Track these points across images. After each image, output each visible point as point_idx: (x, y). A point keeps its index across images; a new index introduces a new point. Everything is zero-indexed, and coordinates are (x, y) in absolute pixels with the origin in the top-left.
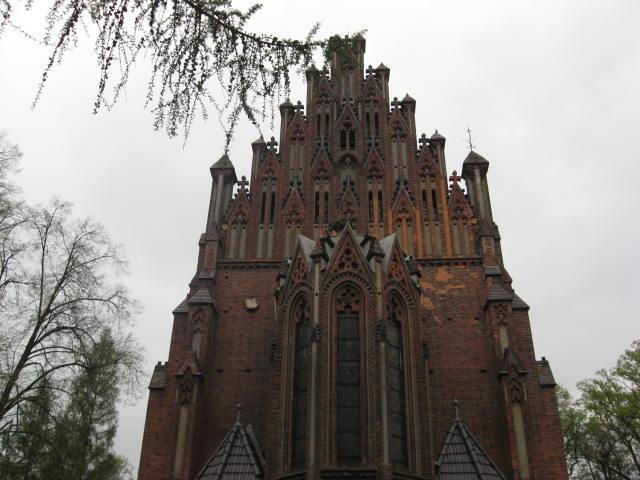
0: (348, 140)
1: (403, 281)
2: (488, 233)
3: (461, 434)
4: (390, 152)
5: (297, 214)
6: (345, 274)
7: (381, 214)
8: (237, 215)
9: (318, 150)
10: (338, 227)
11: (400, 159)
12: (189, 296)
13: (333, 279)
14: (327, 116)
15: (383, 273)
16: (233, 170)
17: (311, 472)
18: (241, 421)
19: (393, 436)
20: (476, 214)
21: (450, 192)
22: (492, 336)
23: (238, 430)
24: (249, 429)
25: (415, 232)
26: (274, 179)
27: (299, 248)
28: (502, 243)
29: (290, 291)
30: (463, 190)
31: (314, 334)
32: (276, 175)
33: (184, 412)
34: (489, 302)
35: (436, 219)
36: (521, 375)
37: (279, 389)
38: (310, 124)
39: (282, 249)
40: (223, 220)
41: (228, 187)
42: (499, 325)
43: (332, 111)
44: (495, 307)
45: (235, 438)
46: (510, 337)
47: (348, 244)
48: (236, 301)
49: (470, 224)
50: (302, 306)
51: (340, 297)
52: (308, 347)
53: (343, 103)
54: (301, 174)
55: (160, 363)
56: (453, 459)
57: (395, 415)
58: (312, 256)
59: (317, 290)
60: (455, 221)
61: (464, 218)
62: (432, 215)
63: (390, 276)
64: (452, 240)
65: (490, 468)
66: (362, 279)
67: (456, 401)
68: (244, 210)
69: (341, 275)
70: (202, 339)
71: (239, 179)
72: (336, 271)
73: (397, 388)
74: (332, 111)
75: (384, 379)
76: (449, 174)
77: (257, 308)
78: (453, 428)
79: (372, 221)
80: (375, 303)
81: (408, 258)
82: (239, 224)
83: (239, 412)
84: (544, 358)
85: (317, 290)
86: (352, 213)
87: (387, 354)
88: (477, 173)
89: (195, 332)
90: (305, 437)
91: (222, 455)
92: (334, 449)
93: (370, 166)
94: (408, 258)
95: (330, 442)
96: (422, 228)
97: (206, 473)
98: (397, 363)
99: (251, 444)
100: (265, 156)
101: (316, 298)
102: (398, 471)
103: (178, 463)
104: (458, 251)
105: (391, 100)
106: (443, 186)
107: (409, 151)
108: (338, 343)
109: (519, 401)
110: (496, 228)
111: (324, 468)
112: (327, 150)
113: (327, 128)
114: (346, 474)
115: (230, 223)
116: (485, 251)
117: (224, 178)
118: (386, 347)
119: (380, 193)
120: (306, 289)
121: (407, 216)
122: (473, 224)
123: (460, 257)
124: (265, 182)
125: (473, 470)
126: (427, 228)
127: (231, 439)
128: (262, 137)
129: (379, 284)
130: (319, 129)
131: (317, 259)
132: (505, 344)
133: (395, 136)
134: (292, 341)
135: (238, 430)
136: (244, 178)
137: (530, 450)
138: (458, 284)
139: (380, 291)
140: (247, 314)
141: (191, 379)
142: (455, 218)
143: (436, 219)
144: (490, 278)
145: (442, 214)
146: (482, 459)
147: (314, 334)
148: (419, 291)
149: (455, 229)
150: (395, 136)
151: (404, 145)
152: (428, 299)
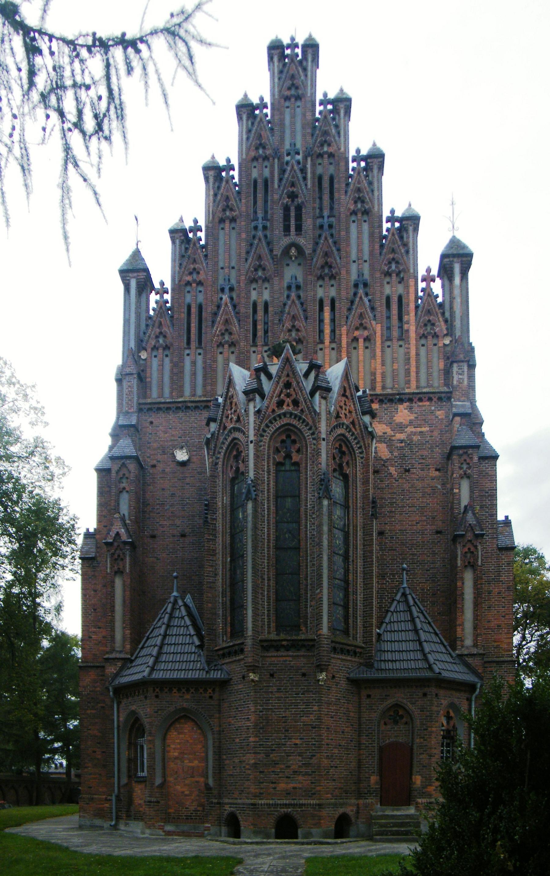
0: (293, 222)
1: (353, 423)
2: (462, 356)
3: (407, 601)
4: (348, 239)
5: (230, 334)
6: (285, 414)
7: (333, 331)
8: (157, 337)
9: (254, 237)
10: (276, 351)
11: (360, 250)
12: (111, 448)
13: (271, 422)
14: (266, 182)
15: (328, 413)
16: (147, 270)
17: (249, 642)
18: (178, 591)
19: (334, 604)
20: (450, 332)
21: (421, 298)
22: (452, 489)
23: (175, 602)
24: (188, 599)
25: (374, 356)
26: (200, 283)
27: (230, 383)
28: (478, 371)
29: (221, 439)
30: (437, 296)
31: (249, 492)
32: (202, 277)
33: (118, 582)
34: (453, 448)
35: (400, 339)
36: (477, 536)
37: (215, 555)
38: (243, 196)
39: (214, 384)
40: (141, 345)
41: (144, 296)
42: (462, 478)
43: (272, 173)
44: (460, 456)
45: (173, 609)
46: (472, 491)
47: (288, 375)
48: (164, 453)
49: (441, 345)
50: (237, 457)
51: (278, 445)
52: (243, 506)
53: (288, 158)
54: (233, 273)
55: (88, 530)
56: (396, 627)
57: (337, 582)
58: (246, 393)
59: (252, 437)
60: (423, 341)
61: (436, 336)
62: (395, 333)
63: (338, 416)
64: (418, 367)
65: (433, 635)
66: (304, 421)
67: (405, 566)
68: (165, 329)
69: (279, 416)
70: (130, 500)
71: (157, 286)
72: (273, 411)
73: (341, 552)
74: (272, 173)
75: (325, 543)
76: (421, 272)
77: (189, 460)
78: (399, 595)
79: (322, 342)
80: (318, 453)
81: (360, 393)
82: (161, 351)
83: (175, 581)
84: (507, 517)
85: (252, 437)
86: (298, 330)
87: (330, 514)
88: (457, 268)
89: (121, 492)
90: (243, 607)
91: (160, 627)
92: (273, 618)
93: (321, 262)
94: (360, 393)
95: (268, 611)
96: (383, 351)
97: (146, 645)
98: (342, 523)
99: (190, 614)
100: (187, 249)
101: (251, 446)
102: (339, 639)
103: (118, 636)
104: (423, 383)
105: (352, 153)
106: (412, 290)
107: (371, 235)
108: (277, 501)
109: (472, 566)
110: (472, 350)
111: (265, 636)
112: (266, 236)
113: (266, 201)
114: (284, 643)
115: (149, 350)
116: (455, 383)
117: (138, 284)
118: (329, 505)
119: (333, 302)
120: (237, 435)
121: (366, 333)
122: (444, 345)
123: (425, 390)
124: (188, 288)
125: (417, 638)
126: (388, 351)
127: (169, 610)
128: (181, 220)
129: (323, 427)
130: (255, 203)
131: (251, 396)
132: (465, 501)
133: (354, 213)
134: (227, 500)
135: (175, 602)
136: (162, 284)
137: (476, 617)
138: (420, 426)
139: (323, 436)
140: (179, 468)
141: (122, 546)
142: (424, 336)
143: (400, 339)
144: (458, 419)
145: (407, 331)
146: (426, 627)
147: (249, 492)
148: (372, 435)
149: (423, 351)
150: (354, 213)
151: (365, 226)
152: (384, 445)
